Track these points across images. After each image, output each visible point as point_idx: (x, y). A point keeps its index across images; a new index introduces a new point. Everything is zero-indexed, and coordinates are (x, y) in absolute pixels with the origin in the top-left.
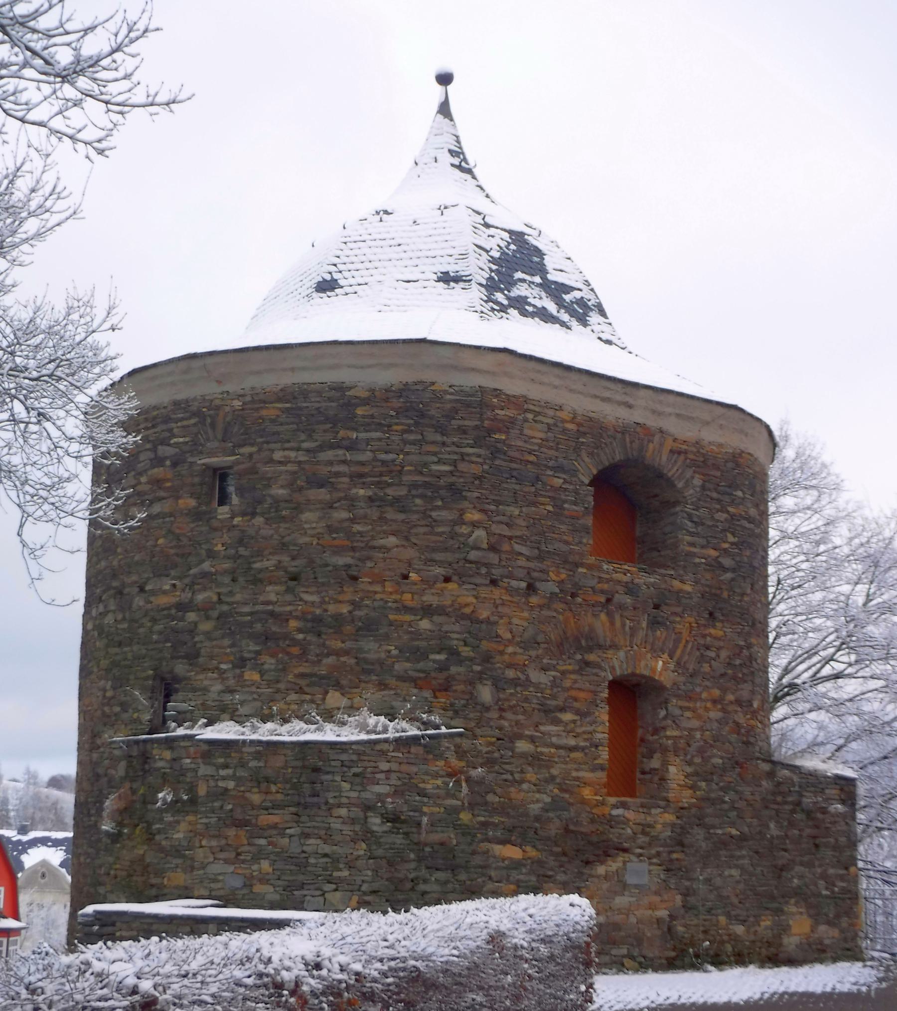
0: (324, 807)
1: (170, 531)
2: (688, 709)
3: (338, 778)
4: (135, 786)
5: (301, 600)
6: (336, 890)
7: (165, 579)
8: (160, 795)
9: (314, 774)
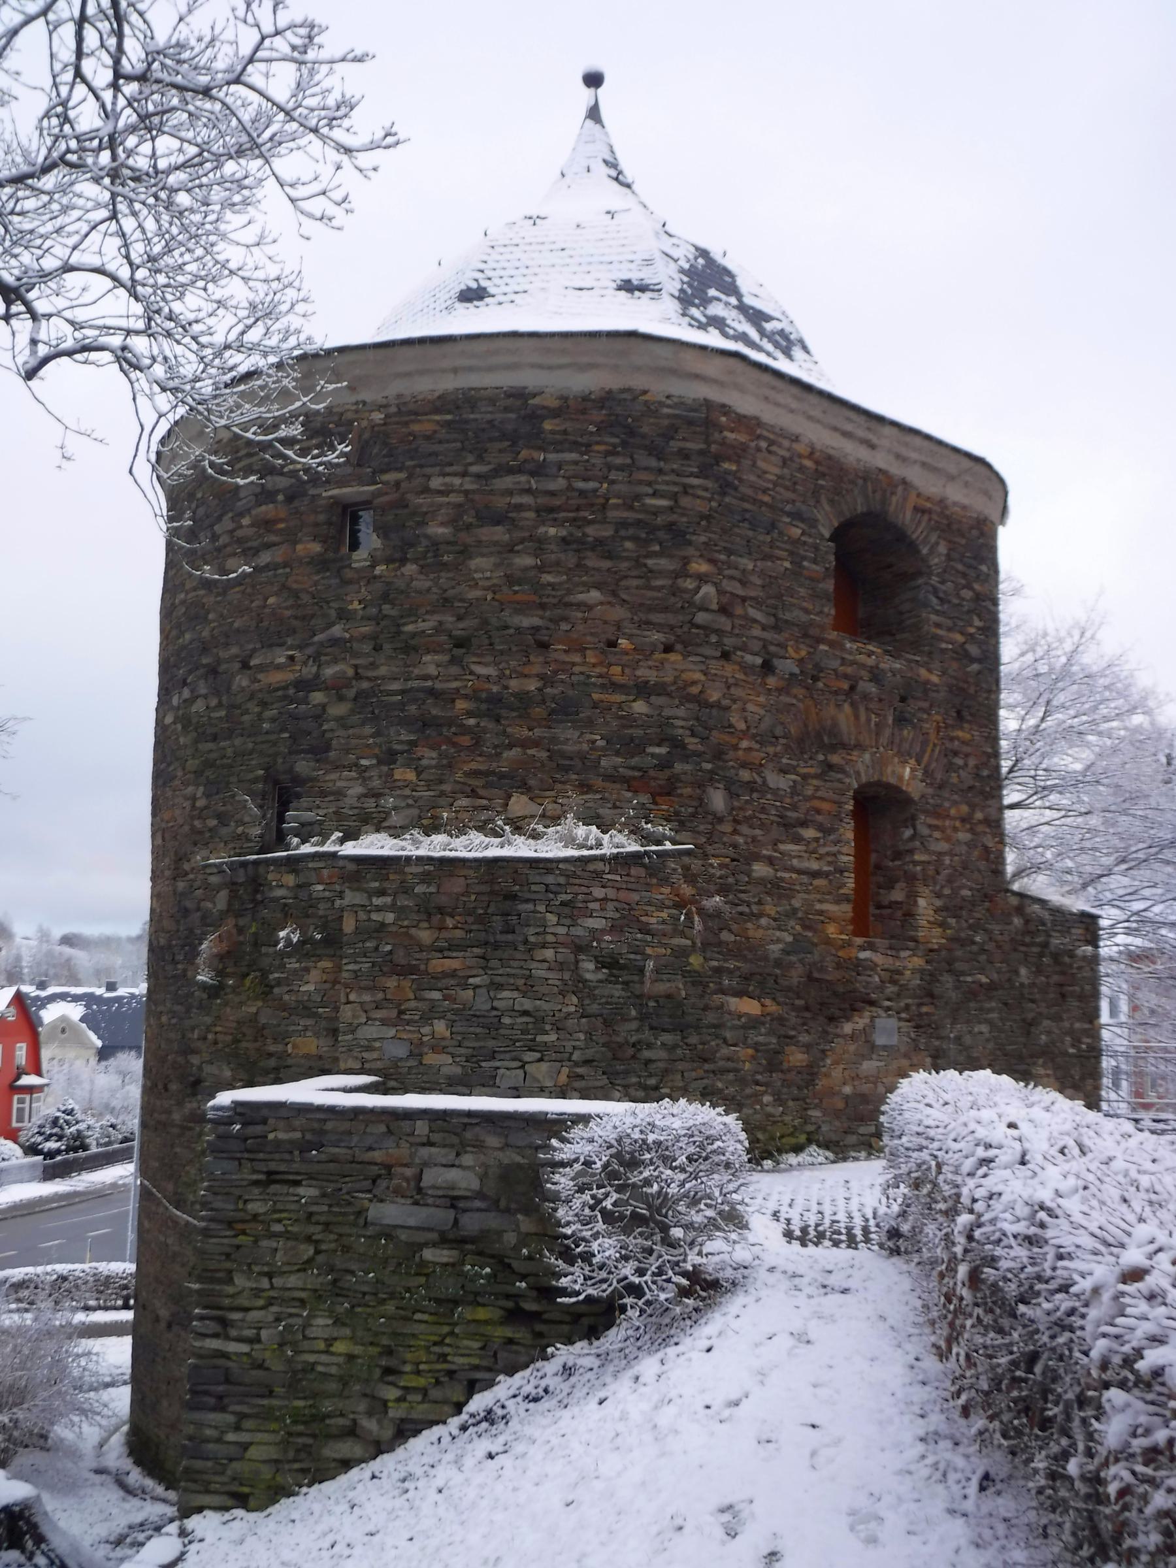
0: (521, 948)
1: (284, 586)
2: (936, 828)
3: (542, 908)
4: (242, 922)
5: (472, 673)
6: (541, 1060)
7: (278, 651)
8: (282, 934)
9: (508, 903)
